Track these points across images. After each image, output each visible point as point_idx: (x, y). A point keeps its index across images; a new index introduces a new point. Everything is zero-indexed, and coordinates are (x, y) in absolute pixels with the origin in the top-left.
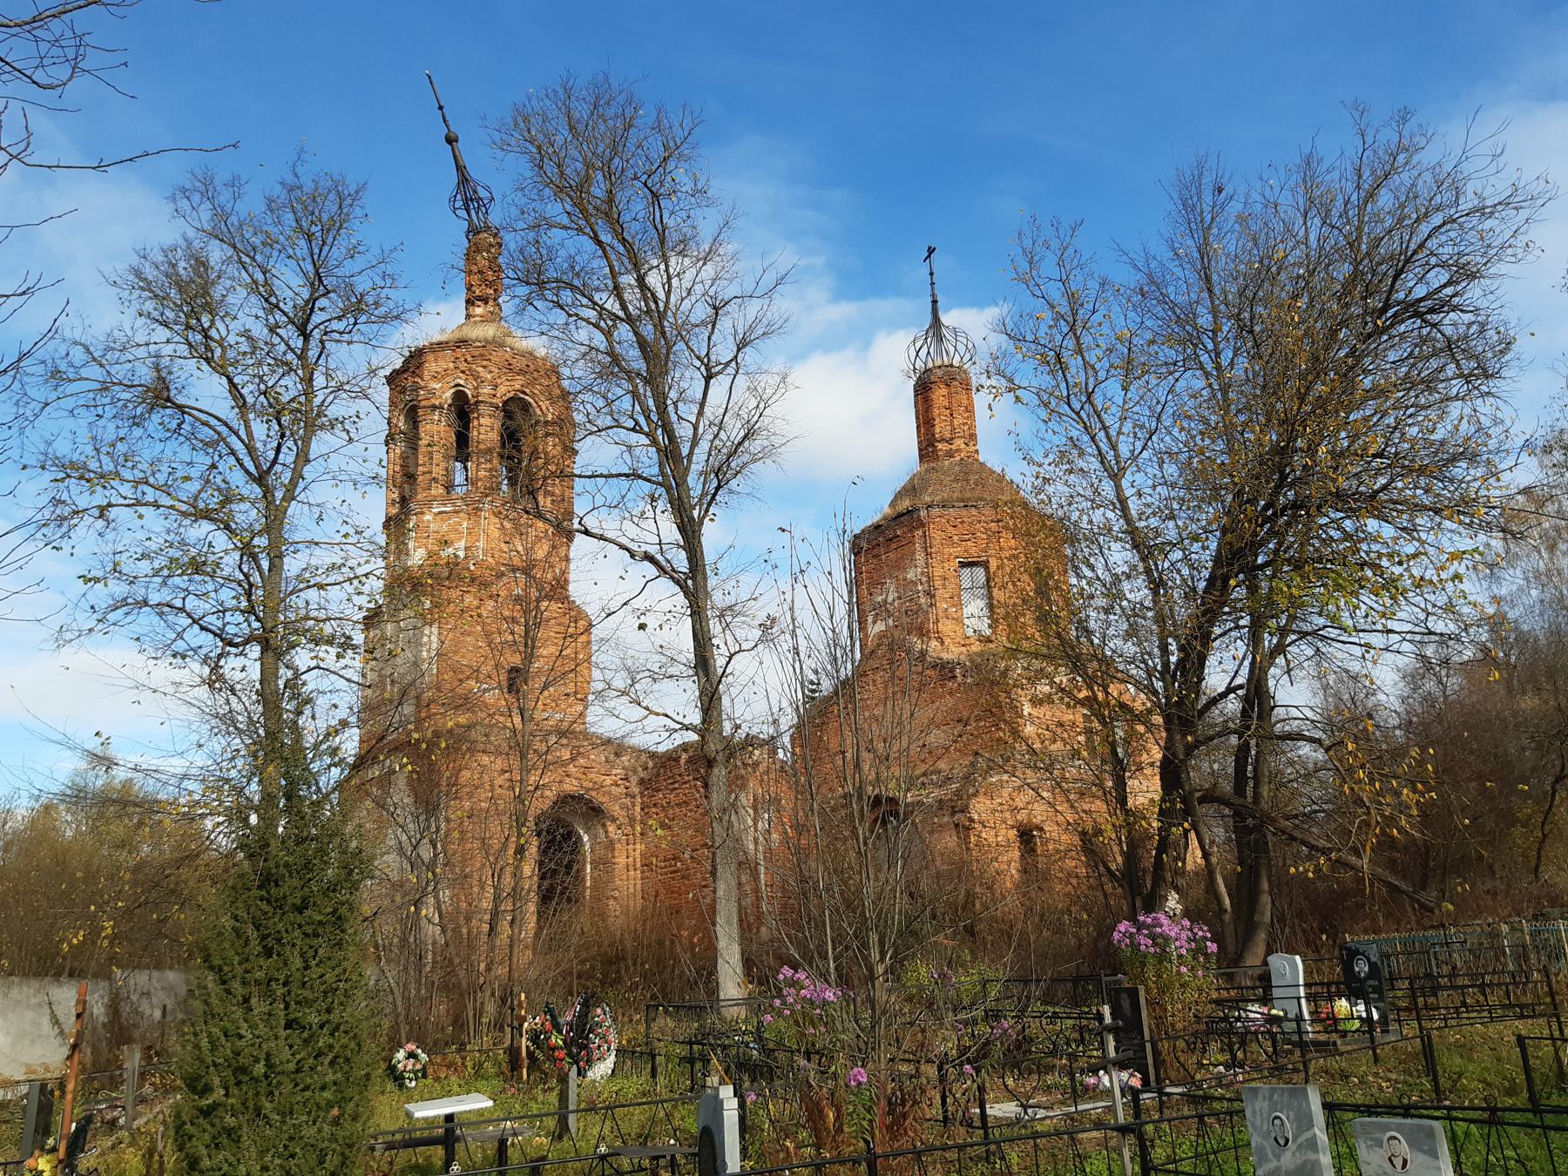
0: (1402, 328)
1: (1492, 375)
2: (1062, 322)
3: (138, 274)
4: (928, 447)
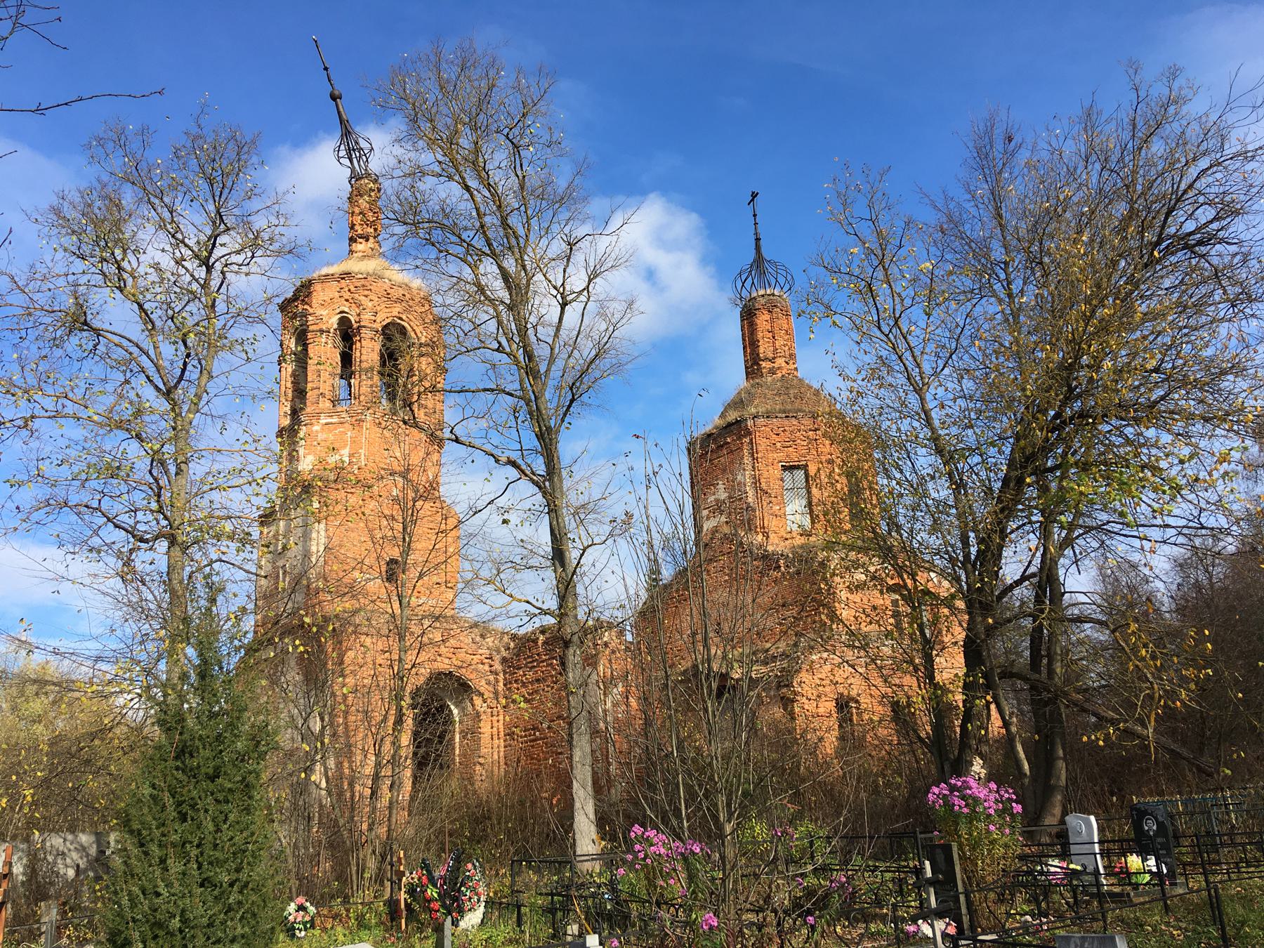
0: (1173, 259)
1: (1255, 299)
2: (873, 256)
3: (57, 211)
4: (753, 366)
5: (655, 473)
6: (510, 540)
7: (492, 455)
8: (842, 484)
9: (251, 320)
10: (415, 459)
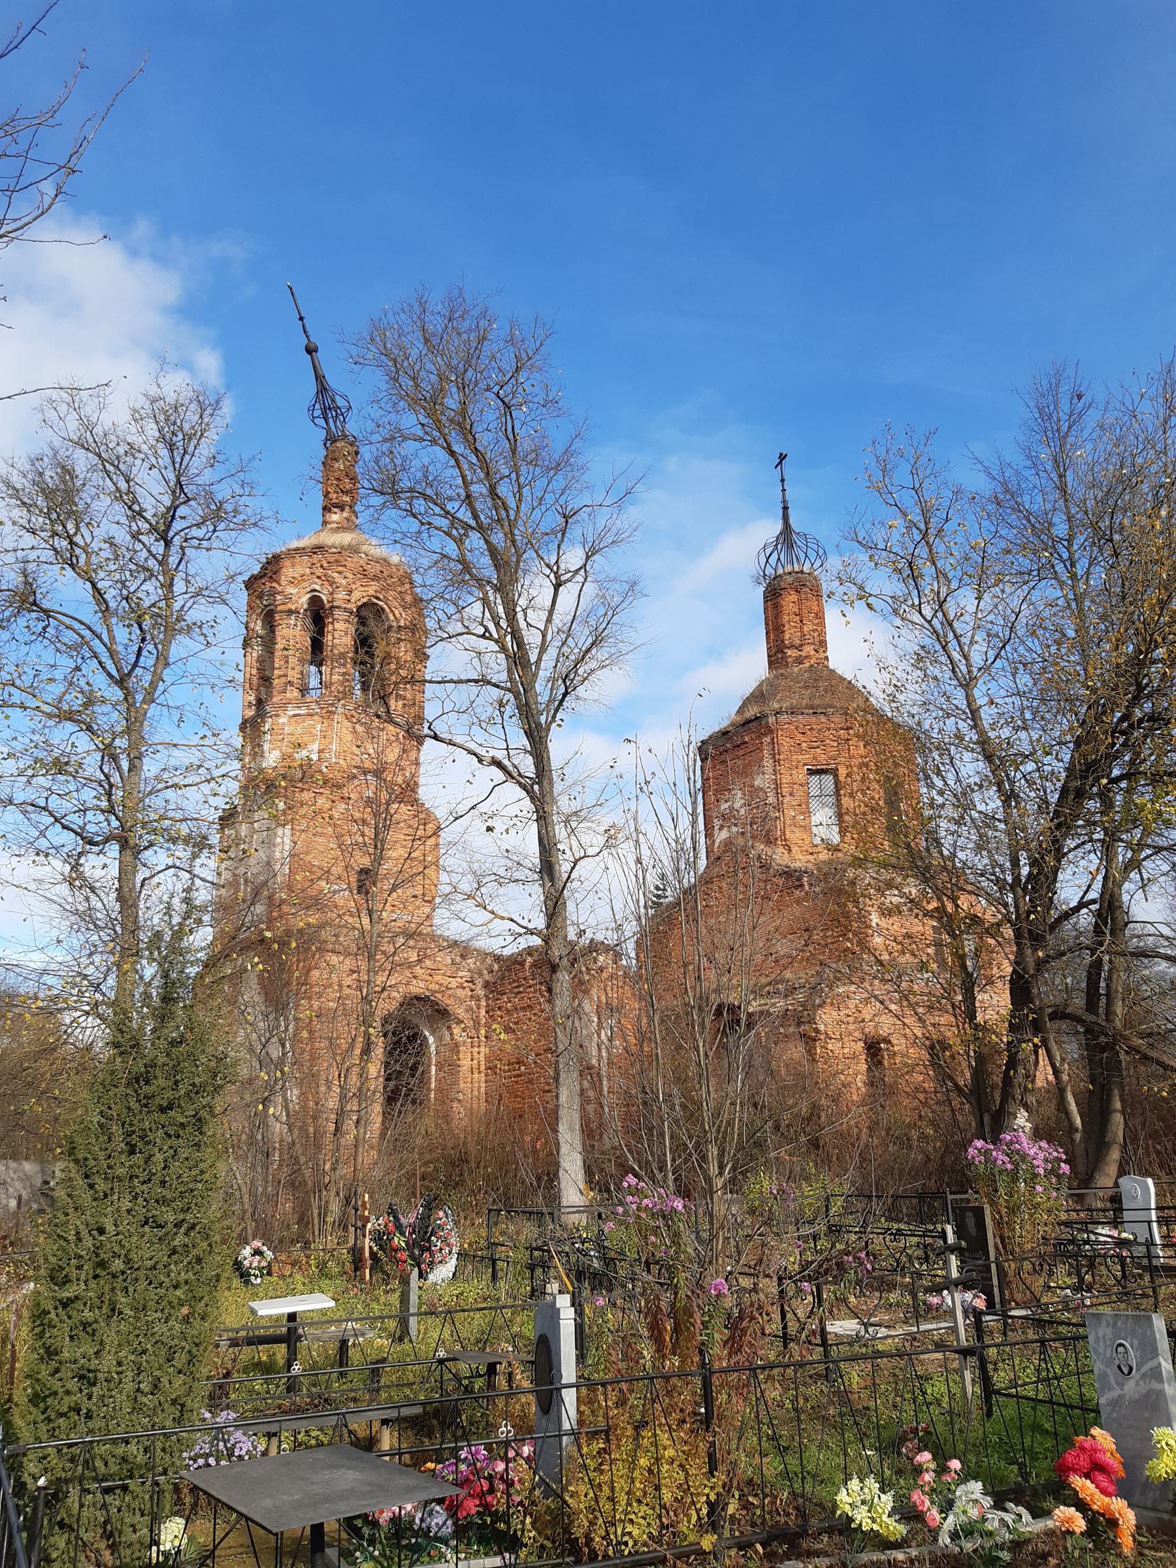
2: (914, 530)
4: (777, 655)
5: (647, 783)
6: (494, 849)
7: (475, 754)
8: (878, 794)
9: (211, 600)
10: (392, 755)
